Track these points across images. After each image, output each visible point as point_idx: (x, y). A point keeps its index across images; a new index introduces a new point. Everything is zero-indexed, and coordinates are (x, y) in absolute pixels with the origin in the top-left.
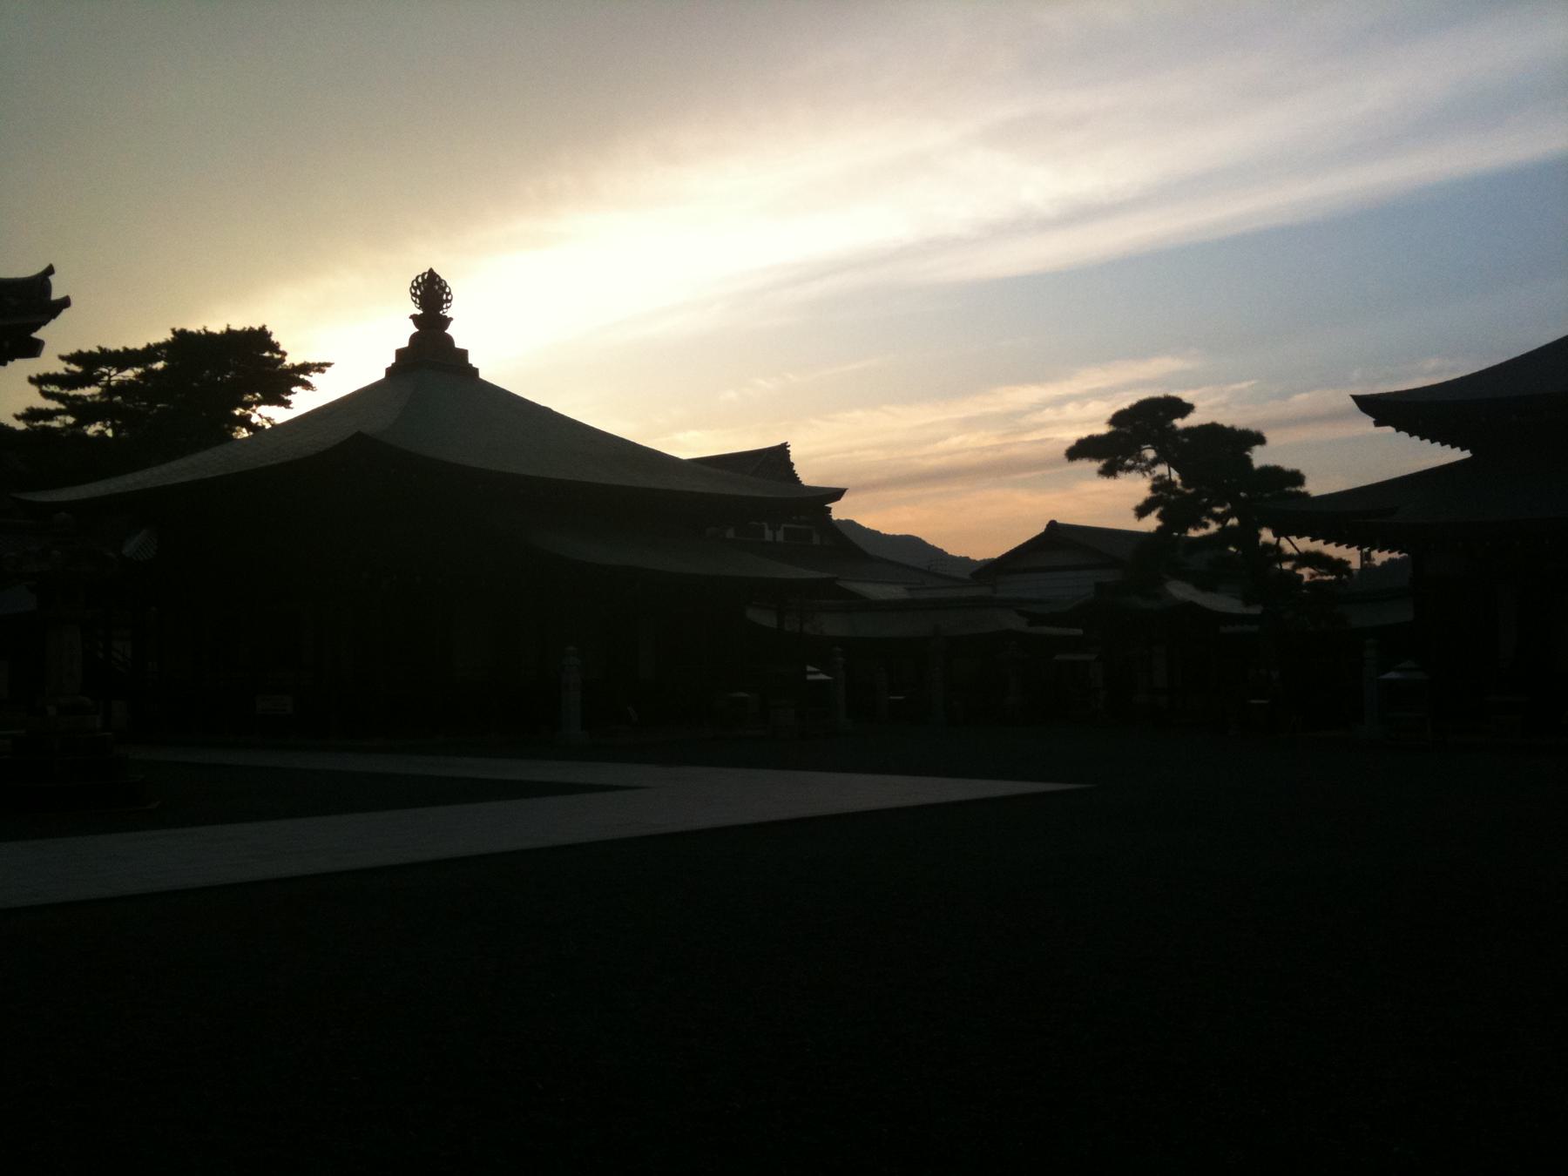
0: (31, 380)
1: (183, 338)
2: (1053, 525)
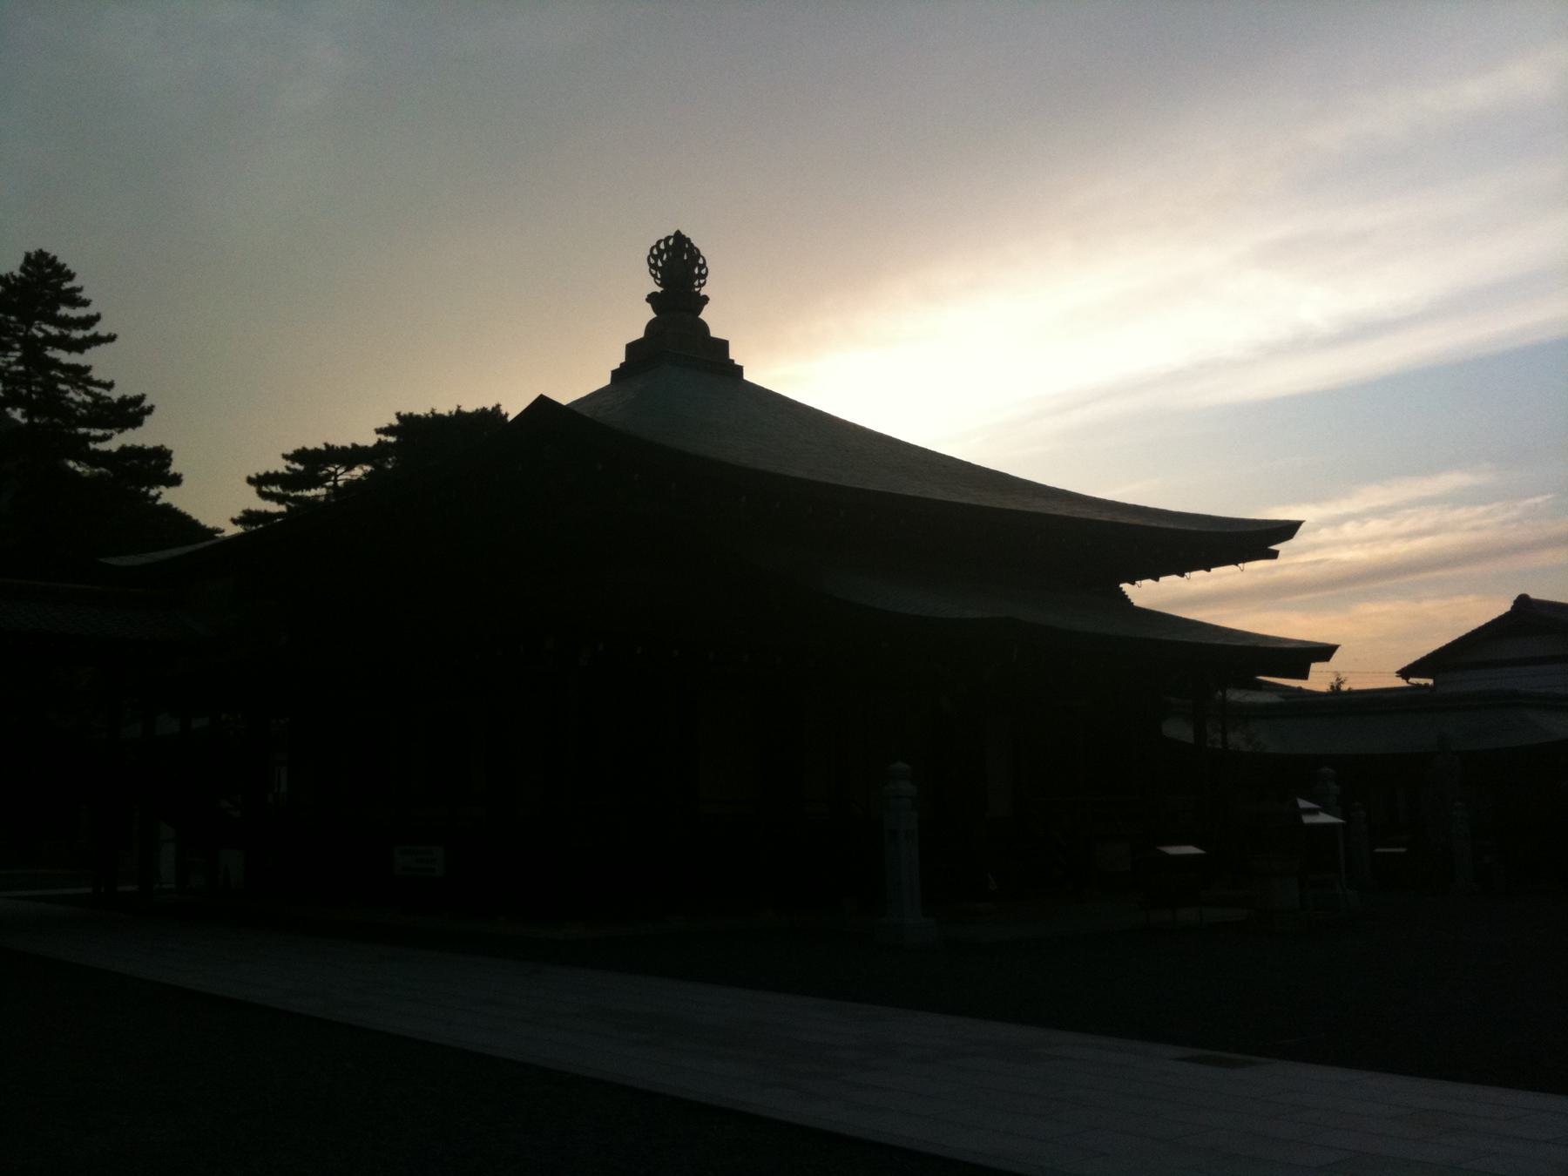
0: (250, 481)
1: (409, 426)
2: (1523, 602)
